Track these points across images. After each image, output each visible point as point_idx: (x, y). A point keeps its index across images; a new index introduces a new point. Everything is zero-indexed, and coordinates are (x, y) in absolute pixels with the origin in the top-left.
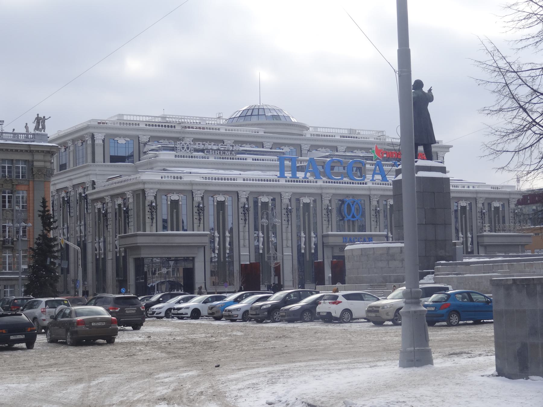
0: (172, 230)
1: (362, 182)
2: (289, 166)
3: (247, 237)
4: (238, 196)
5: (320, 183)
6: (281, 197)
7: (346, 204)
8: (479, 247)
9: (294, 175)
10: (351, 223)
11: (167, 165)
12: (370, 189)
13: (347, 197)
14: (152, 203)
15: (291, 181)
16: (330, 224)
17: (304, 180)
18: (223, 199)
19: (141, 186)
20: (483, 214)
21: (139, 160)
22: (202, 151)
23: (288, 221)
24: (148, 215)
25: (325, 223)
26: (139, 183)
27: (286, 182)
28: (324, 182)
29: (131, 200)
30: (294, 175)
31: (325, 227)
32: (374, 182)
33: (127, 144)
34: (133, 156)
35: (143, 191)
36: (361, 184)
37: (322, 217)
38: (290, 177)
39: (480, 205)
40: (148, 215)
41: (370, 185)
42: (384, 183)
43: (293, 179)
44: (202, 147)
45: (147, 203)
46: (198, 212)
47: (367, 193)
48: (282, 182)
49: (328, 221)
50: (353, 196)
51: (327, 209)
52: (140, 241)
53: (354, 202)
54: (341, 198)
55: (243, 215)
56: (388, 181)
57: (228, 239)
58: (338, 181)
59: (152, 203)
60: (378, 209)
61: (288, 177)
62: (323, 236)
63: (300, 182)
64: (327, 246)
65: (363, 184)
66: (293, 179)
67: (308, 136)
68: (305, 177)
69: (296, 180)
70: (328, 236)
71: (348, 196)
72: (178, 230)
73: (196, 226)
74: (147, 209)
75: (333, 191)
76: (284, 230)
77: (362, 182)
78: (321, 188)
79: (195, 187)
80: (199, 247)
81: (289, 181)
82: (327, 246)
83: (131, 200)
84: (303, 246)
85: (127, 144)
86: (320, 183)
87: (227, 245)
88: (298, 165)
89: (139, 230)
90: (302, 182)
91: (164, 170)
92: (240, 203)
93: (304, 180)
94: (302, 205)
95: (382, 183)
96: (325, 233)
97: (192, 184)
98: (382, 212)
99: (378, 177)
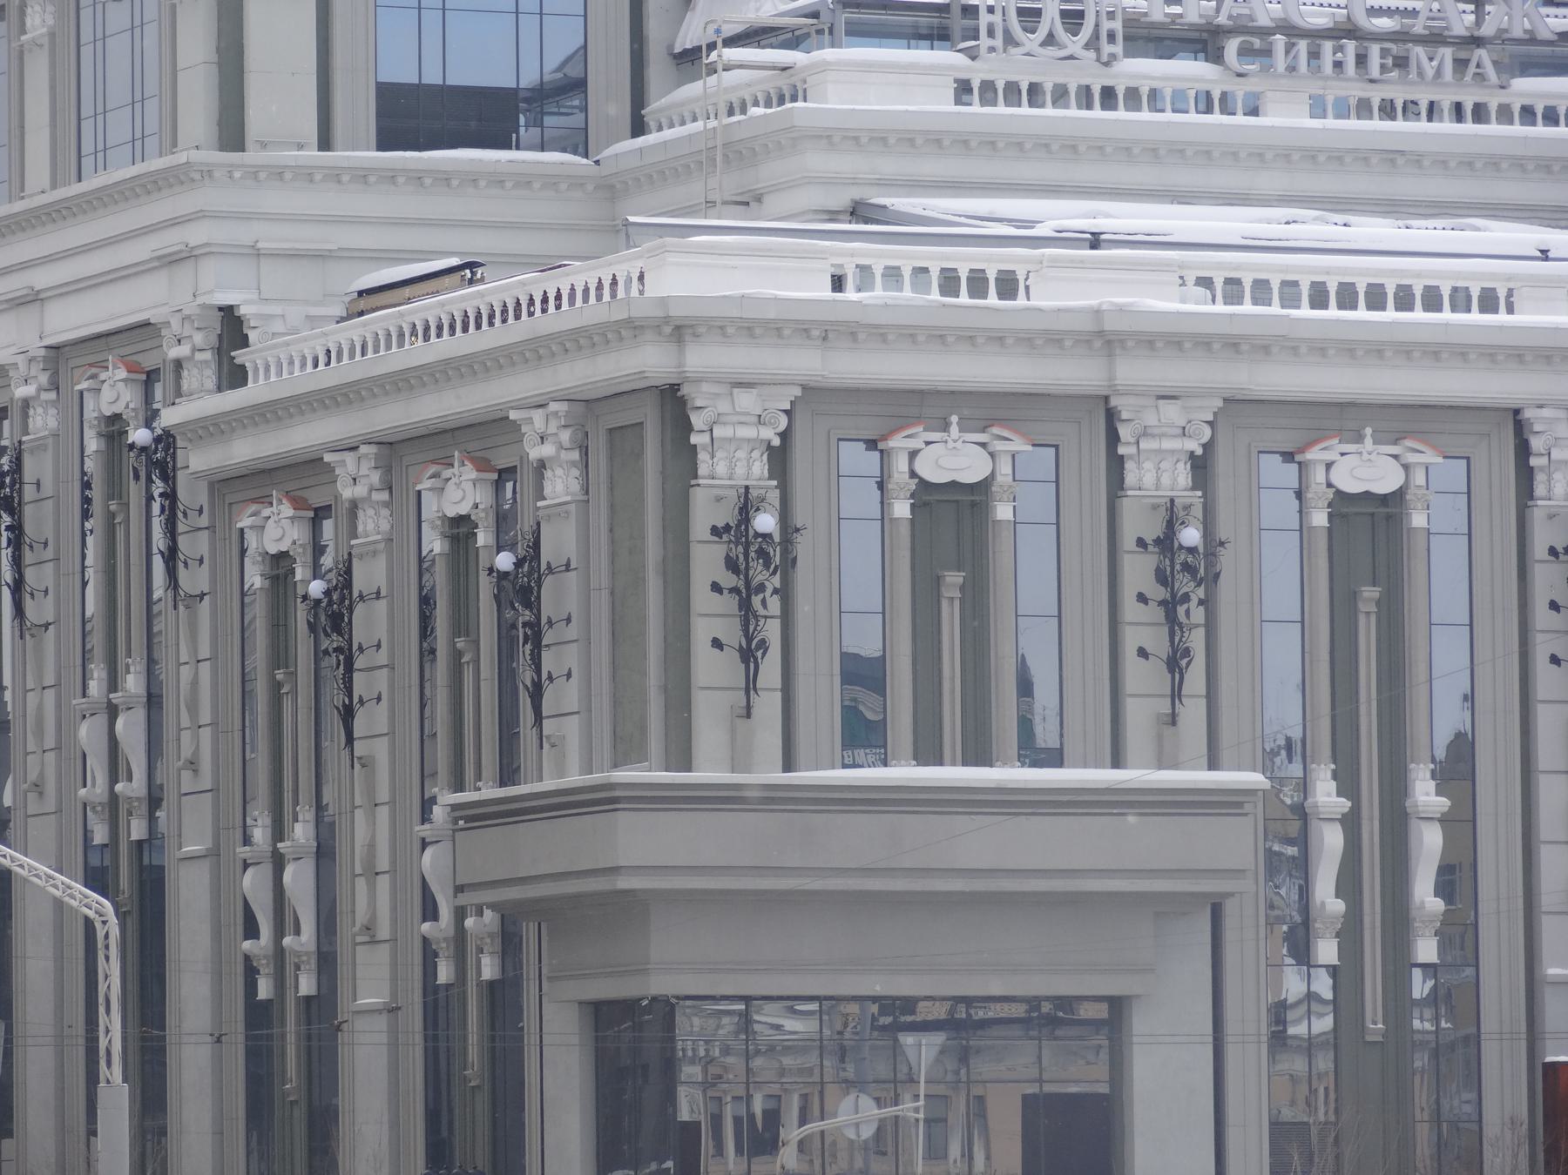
0: (929, 753)
4: (1523, 450)
11: (889, 166)
14: (747, 508)
18: (1385, 480)
19: (650, 361)
21: (639, 128)
24: (712, 617)
26: (631, 329)
29: (561, 486)
34: (579, 85)
35: (672, 400)
40: (712, 617)
45: (706, 513)
46: (1158, 592)
51: (1166, 542)
52: (641, 847)
55: (730, 603)
57: (1429, 843)
59: (747, 508)
72: (978, 754)
73: (1140, 715)
74: (708, 561)
79: (1133, 372)
83: (561, 486)
87: (1425, 896)
89: (627, 749)
91: (858, 211)
92: (1538, 515)
97: (1105, 338)
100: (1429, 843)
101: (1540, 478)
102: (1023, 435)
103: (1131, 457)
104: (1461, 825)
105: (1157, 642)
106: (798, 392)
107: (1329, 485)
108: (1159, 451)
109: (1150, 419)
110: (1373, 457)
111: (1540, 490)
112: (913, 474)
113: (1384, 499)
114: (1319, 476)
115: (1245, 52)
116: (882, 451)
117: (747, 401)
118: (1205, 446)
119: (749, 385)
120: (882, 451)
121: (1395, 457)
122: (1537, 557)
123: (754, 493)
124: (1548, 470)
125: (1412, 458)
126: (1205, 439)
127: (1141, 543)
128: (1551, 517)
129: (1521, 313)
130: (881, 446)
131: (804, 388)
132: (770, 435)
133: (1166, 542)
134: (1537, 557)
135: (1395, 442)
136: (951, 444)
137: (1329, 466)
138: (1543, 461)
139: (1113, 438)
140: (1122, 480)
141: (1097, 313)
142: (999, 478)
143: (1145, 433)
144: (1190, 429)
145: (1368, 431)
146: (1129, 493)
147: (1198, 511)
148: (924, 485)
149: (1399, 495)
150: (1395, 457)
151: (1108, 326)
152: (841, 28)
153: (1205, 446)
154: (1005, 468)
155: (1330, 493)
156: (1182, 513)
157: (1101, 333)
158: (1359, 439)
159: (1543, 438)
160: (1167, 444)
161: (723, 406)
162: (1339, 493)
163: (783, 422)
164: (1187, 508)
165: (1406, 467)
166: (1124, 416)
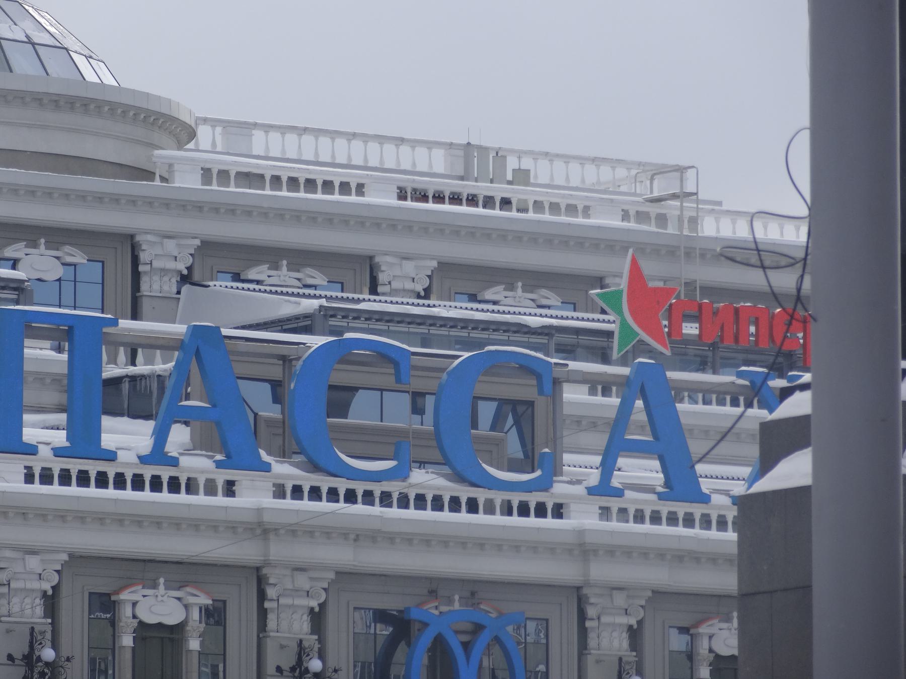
2: (56, 379)
5: (254, 496)
9: (84, 440)
12: (583, 549)
13: (433, 593)
14: (302, 652)
15: (65, 478)
17: (148, 472)
27: (29, 478)
28: (279, 492)
30: (84, 440)
32: (614, 504)
33: (68, 287)
36: (524, 510)
38: (58, 452)
41: (584, 519)
42: (681, 509)
43: (75, 466)
47: (563, 571)
50: (473, 589)
53: (478, 628)
54: (391, 603)
56: (705, 499)
61: (45, 452)
63: (120, 481)
65: (541, 511)
66: (75, 466)
67: (187, 181)
68: (158, 454)
69: (93, 468)
71: (434, 587)
75: (343, 556)
77: (533, 499)
78: (261, 528)
79: (280, 551)
81: (46, 477)
85: (68, 287)
86: (254, 496)
88: (110, 371)
90: (138, 483)
92: (590, 660)
93: (148, 472)
94: (127, 641)
95: (665, 508)
99: (641, 471)
102: (207, 593)
103: (272, 610)
106: (65, 557)
107: (134, 617)
108: (614, 624)
110: (165, 598)
112: (711, 651)
113: (172, 628)
114: (128, 611)
116: (692, 635)
117: (33, 563)
118: (53, 588)
119: (33, 552)
120: (692, 635)
121: (179, 599)
122: (269, 673)
123: (624, 659)
125: (191, 600)
126: (54, 584)
127: (279, 669)
128: (598, 662)
129: (569, 518)
130: (692, 631)
131: (653, 592)
132: (47, 586)
134: (269, 673)
135: (179, 589)
136: (160, 598)
137: (134, 604)
138: (274, 605)
139: (262, 596)
140: (266, 625)
142: (191, 623)
144: (44, 575)
145: (162, 580)
146: (272, 634)
147: (49, 636)
148: (718, 657)
150: (179, 599)
151: (266, 518)
153: (53, 588)
154: (195, 615)
155: (135, 623)
156: (39, 637)
157: (260, 524)
158: (155, 586)
159: (277, 588)
160: (298, 602)
161: (19, 568)
162: (141, 623)
163: (55, 579)
164: (43, 633)
165: (186, 607)
166: (271, 581)
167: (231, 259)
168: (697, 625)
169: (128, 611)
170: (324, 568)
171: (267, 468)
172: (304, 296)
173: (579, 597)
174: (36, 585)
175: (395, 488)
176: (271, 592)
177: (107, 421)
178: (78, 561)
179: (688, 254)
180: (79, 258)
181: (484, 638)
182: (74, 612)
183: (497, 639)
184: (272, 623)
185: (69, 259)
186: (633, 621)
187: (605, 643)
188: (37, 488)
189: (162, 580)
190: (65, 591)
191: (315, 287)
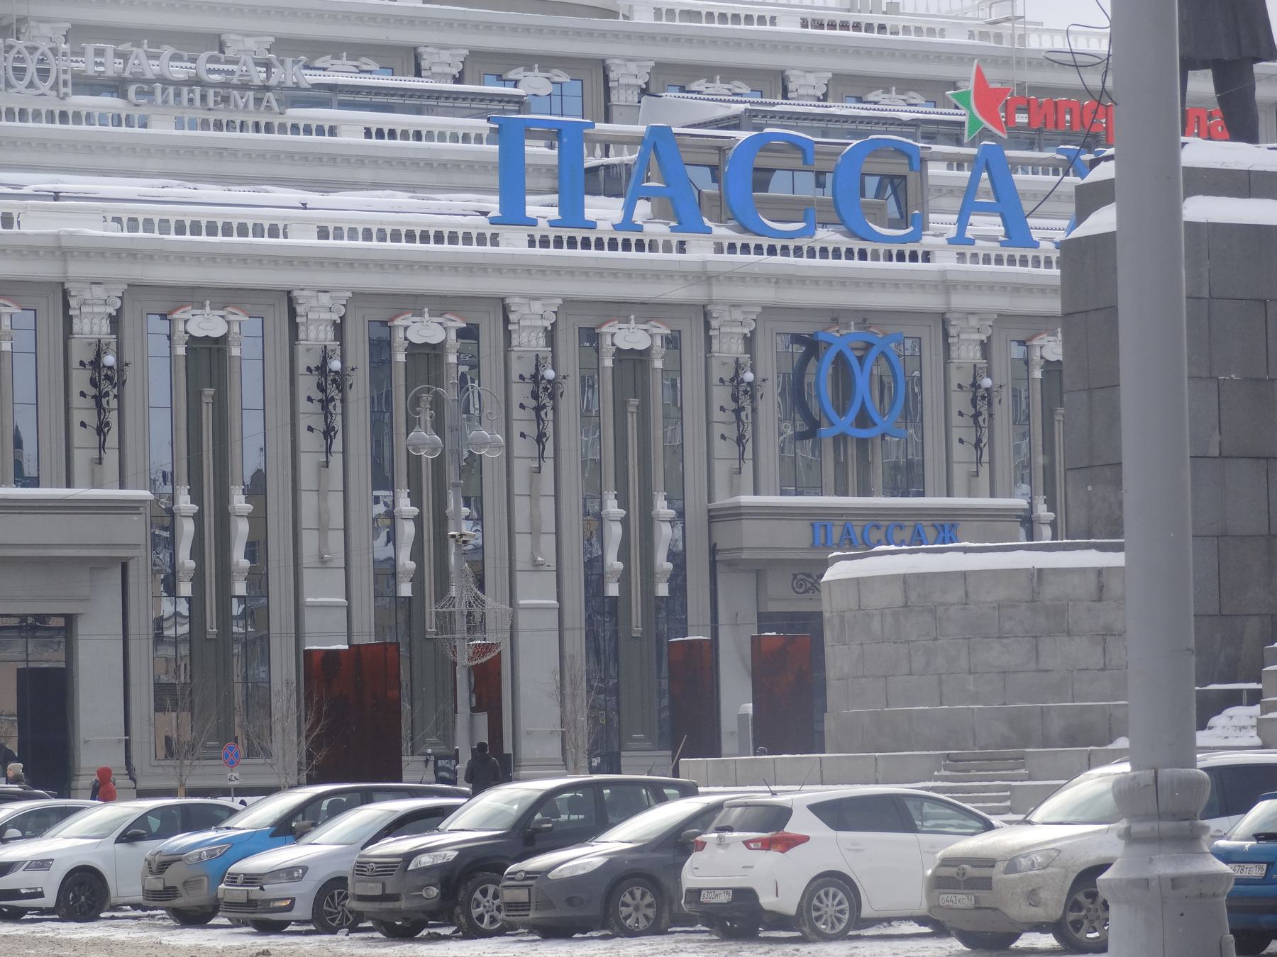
1: (907, 248)
2: (549, 169)
3: (337, 521)
4: (292, 313)
5: (700, 252)
6: (507, 321)
7: (830, 356)
8: (720, 568)
9: (572, 214)
10: (852, 450)
12: (946, 285)
13: (835, 321)
14: (738, 367)
15: (558, 243)
16: (985, 458)
17: (620, 236)
20: (980, 398)
22: (117, 87)
23: (740, 440)
25: (723, 449)
27: (532, 243)
28: (719, 249)
30: (572, 214)
31: (721, 470)
32: (968, 250)
33: (556, 100)
36: (901, 257)
37: (709, 423)
38: (553, 224)
39: (729, 347)
41: (946, 262)
42: (1018, 253)
43: (565, 233)
44: (112, 68)
48: (514, 243)
49: (740, 440)
50: (865, 317)
51: (736, 379)
53: (869, 346)
54: (804, 329)
57: (241, 529)
58: (792, 244)
59: (325, 359)
60: (987, 382)
61: (543, 223)
62: (714, 517)
63: (599, 244)
64: (733, 565)
65: (914, 257)
66: (565, 233)
68: (627, 223)
69: (579, 234)
70: (736, 514)
71: (836, 316)
72: (865, 491)
73: (81, 459)
75: (767, 294)
76: (520, 486)
77: (907, 248)
78: (705, 276)
79: (77, 269)
80: (95, 565)
81: (544, 243)
82: (733, 565)
84: (613, 562)
85: (556, 100)
86: (700, 252)
87: (239, 558)
88: (590, 162)
90: (613, 245)
92: (953, 367)
93: (620, 236)
95: (1006, 253)
96: (722, 500)
97: (61, 250)
98: (1006, 395)
99: (987, 225)
100: (241, 529)
101: (953, 349)
104: (259, 520)
105: (91, 418)
109: (87, 296)
111: (302, 335)
115: (140, 93)
124: (306, 325)
132: (547, 324)
133: (736, 379)
135: (441, 316)
141: (57, 236)
143: (84, 303)
148: (1047, 361)
149: (224, 338)
151: (710, 268)
152: (334, 103)
154: (453, 335)
157: (705, 273)
167: (677, 76)
168: (1031, 339)
169: (608, 341)
170: (753, 304)
171: (708, 231)
172: (733, 102)
173: (943, 320)
174: (539, 323)
175: (804, 243)
176: (714, 323)
177: (588, 199)
178: (569, 304)
179: (1018, 63)
180: (564, 78)
181: (874, 353)
182: (568, 343)
183: (883, 353)
184: (715, 347)
185: (557, 79)
186: (336, 317)
187: (312, 335)
188: (538, 250)
189: (208, 302)
190: (560, 326)
191: (741, 95)
